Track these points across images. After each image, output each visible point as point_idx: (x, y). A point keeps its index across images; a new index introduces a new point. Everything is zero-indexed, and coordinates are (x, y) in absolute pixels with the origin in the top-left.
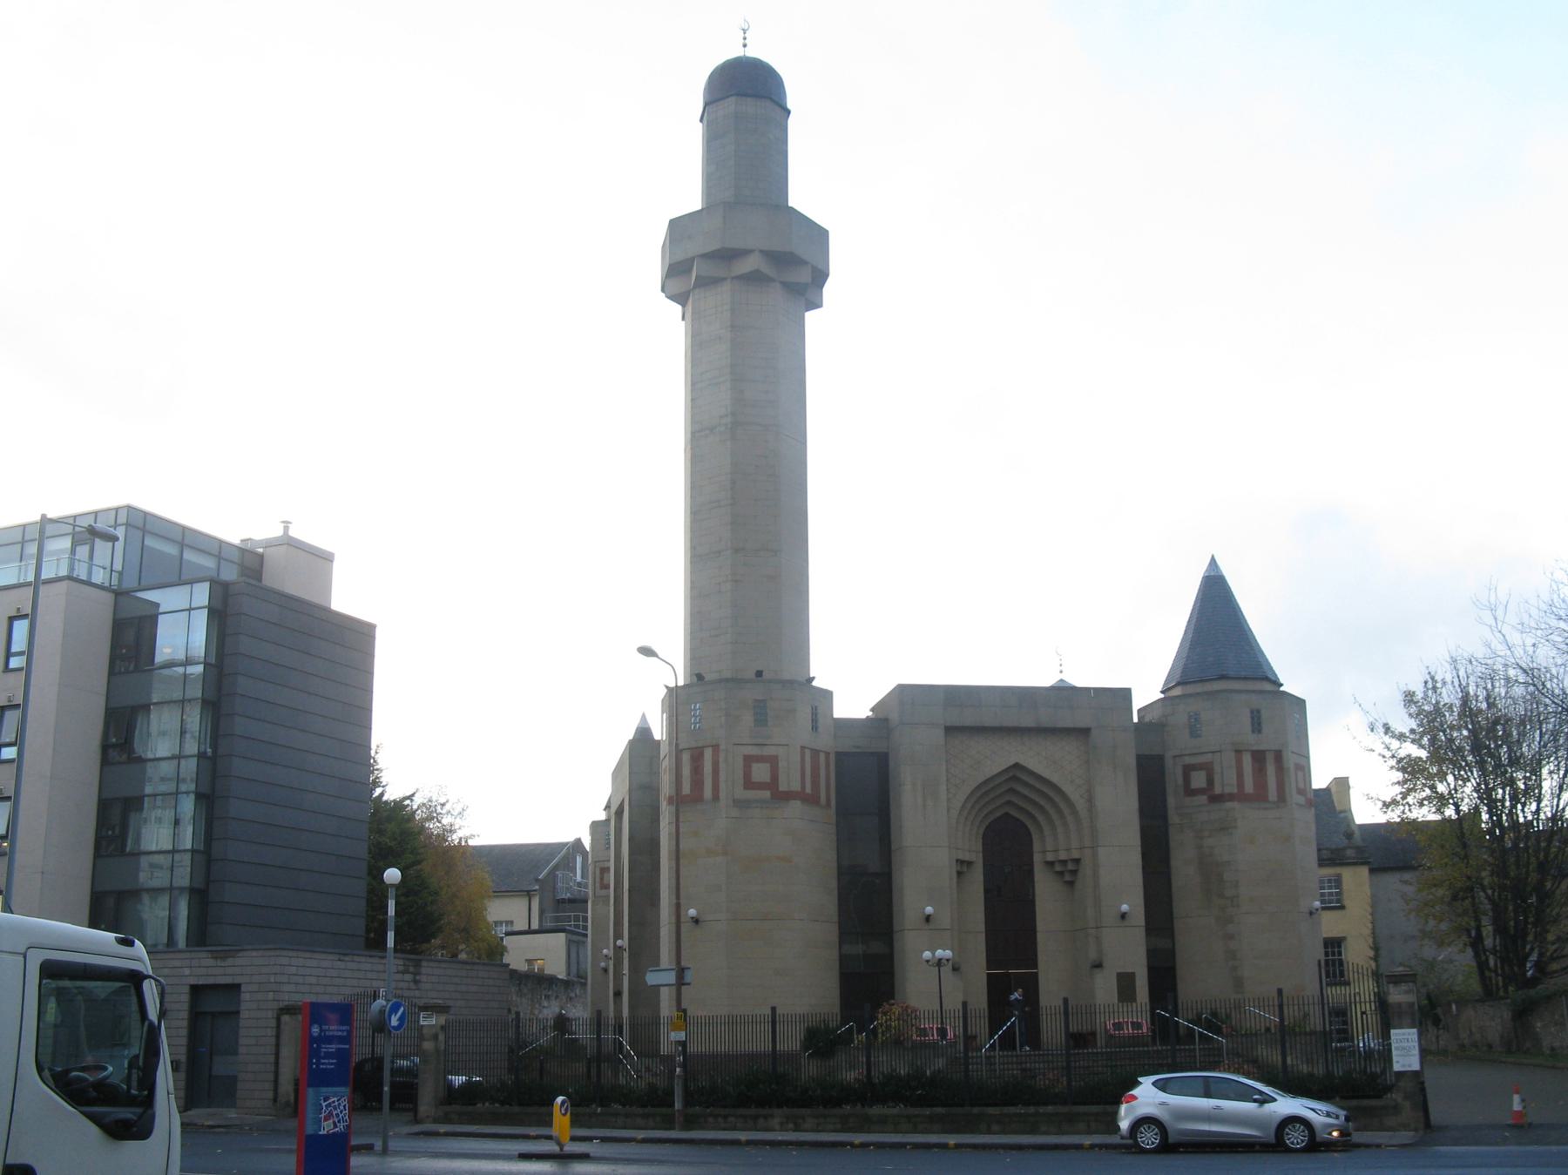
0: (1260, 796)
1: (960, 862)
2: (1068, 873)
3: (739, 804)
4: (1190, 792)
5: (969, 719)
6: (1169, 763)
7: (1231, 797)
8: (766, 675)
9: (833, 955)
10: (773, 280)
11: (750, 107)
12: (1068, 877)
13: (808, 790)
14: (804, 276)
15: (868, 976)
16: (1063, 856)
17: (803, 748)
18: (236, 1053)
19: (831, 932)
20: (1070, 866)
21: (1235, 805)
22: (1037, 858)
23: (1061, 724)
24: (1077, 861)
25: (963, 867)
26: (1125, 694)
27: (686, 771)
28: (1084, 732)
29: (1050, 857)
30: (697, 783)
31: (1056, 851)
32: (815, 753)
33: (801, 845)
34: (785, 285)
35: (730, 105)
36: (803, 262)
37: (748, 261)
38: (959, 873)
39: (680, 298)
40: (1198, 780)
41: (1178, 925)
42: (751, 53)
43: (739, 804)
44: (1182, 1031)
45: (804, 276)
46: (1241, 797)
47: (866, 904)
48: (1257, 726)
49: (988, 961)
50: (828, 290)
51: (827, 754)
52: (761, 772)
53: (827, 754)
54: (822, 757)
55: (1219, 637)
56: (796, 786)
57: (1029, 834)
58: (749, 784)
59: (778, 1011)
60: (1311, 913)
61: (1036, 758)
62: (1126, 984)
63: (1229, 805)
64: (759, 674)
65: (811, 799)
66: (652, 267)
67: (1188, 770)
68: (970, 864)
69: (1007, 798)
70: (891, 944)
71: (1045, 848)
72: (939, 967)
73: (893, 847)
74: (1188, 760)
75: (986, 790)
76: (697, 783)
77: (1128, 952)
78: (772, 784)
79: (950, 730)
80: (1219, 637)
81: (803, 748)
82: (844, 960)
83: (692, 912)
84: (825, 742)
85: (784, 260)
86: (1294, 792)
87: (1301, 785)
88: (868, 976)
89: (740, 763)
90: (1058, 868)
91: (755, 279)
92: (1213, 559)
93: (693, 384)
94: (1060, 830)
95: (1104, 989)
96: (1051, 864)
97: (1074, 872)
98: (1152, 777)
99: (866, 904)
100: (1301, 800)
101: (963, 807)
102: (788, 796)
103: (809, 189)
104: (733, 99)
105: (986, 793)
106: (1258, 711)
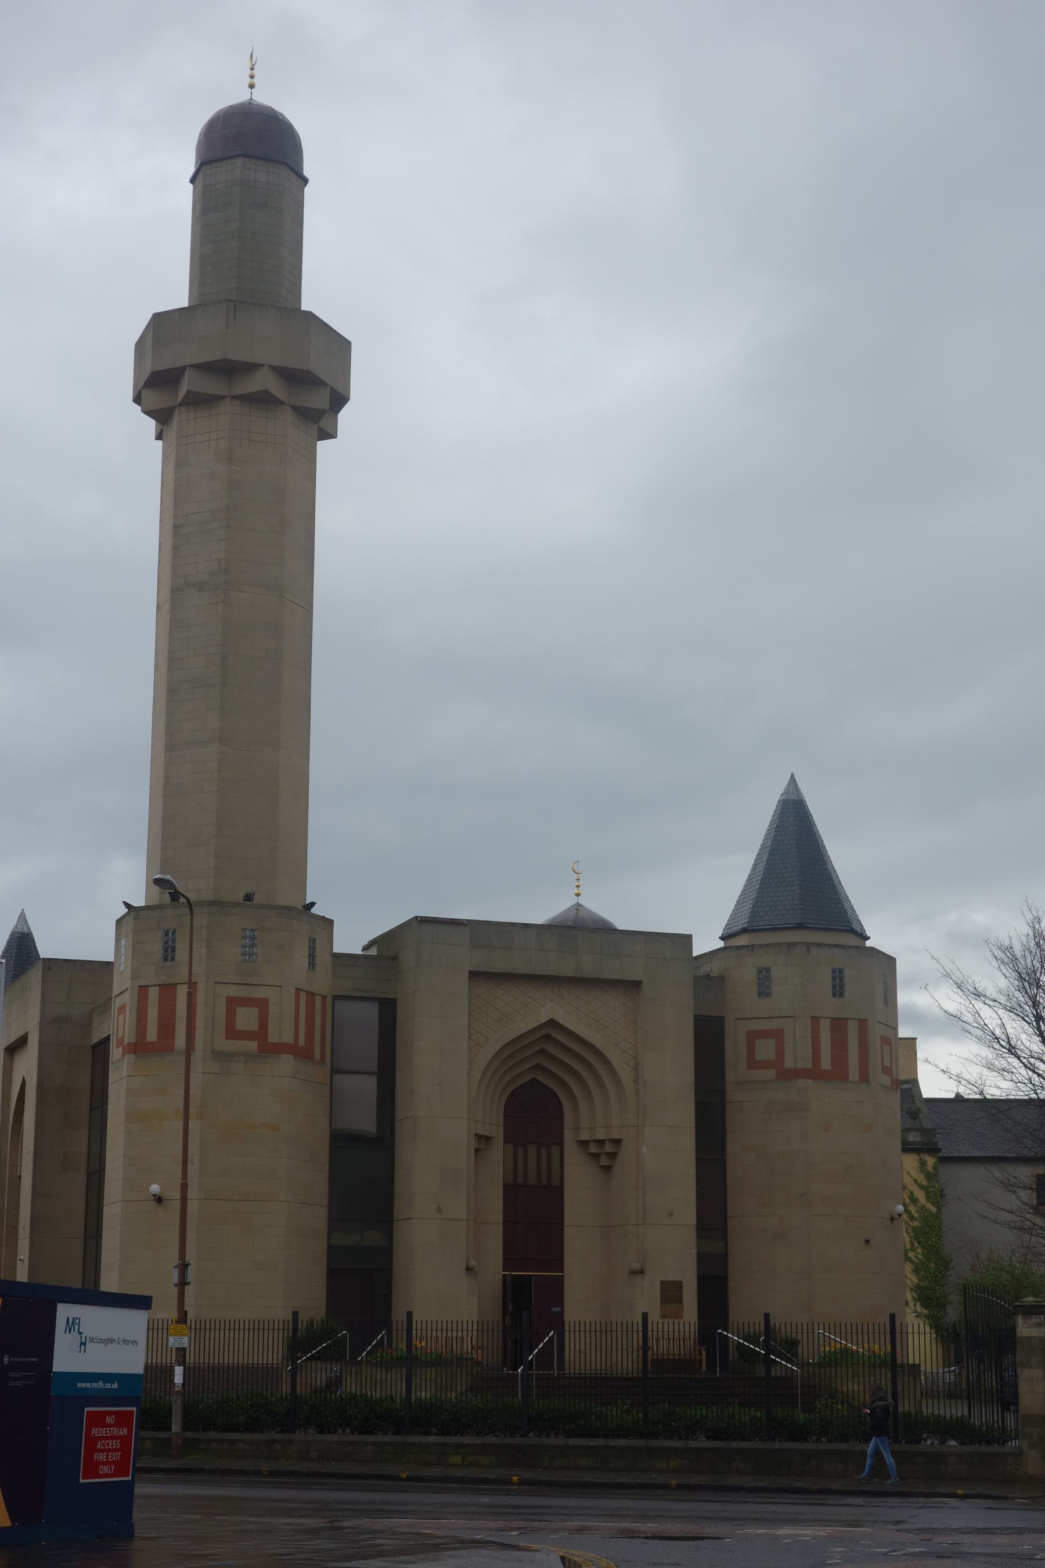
0: (838, 1074)
1: (479, 1137)
2: (605, 1155)
3: (219, 1056)
4: (753, 1063)
5: (499, 964)
6: (729, 1027)
7: (804, 1074)
8: (258, 899)
9: (321, 1246)
10: (282, 403)
11: (262, 174)
12: (604, 1161)
13: (302, 1042)
14: (320, 400)
15: (360, 1280)
16: (600, 1136)
17: (298, 990)
19: (320, 1217)
20: (609, 1148)
22: (568, 1135)
23: (607, 975)
24: (617, 1142)
25: (483, 1141)
26: (687, 940)
27: (153, 1014)
29: (584, 1136)
30: (167, 1028)
32: (311, 996)
33: (279, 1114)
34: (295, 408)
35: (236, 170)
36: (321, 383)
37: (242, 371)
38: (477, 1150)
39: (162, 417)
40: (765, 1050)
41: (731, 1223)
42: (263, 97)
43: (219, 1056)
44: (733, 1354)
45: (320, 400)
46: (814, 1073)
47: (362, 1174)
48: (838, 988)
49: (506, 1260)
50: (344, 416)
51: (324, 998)
52: (247, 1019)
53: (324, 998)
55: (797, 884)
56: (288, 1038)
57: (561, 1118)
58: (232, 1033)
60: (892, 1219)
61: (569, 1012)
62: (671, 1293)
63: (801, 1082)
65: (303, 1054)
66: (123, 375)
67: (752, 1037)
69: (534, 1062)
70: (389, 1234)
71: (584, 1120)
72: (445, 1281)
73: (399, 1115)
74: (754, 1025)
76: (167, 1028)
77: (677, 1258)
78: (261, 1034)
80: (797, 884)
81: (298, 990)
82: (333, 1251)
84: (323, 983)
85: (297, 378)
86: (879, 1069)
87: (887, 1063)
88: (360, 1280)
89: (222, 1007)
90: (593, 1149)
91: (262, 400)
92: (792, 775)
93: (176, 527)
94: (595, 1091)
95: (646, 1299)
96: (584, 1144)
97: (613, 1156)
98: (709, 1037)
99: (362, 1174)
100: (886, 1080)
101: (484, 1073)
102: (279, 1049)
103: (327, 285)
104: (239, 161)
105: (511, 1056)
106: (841, 971)
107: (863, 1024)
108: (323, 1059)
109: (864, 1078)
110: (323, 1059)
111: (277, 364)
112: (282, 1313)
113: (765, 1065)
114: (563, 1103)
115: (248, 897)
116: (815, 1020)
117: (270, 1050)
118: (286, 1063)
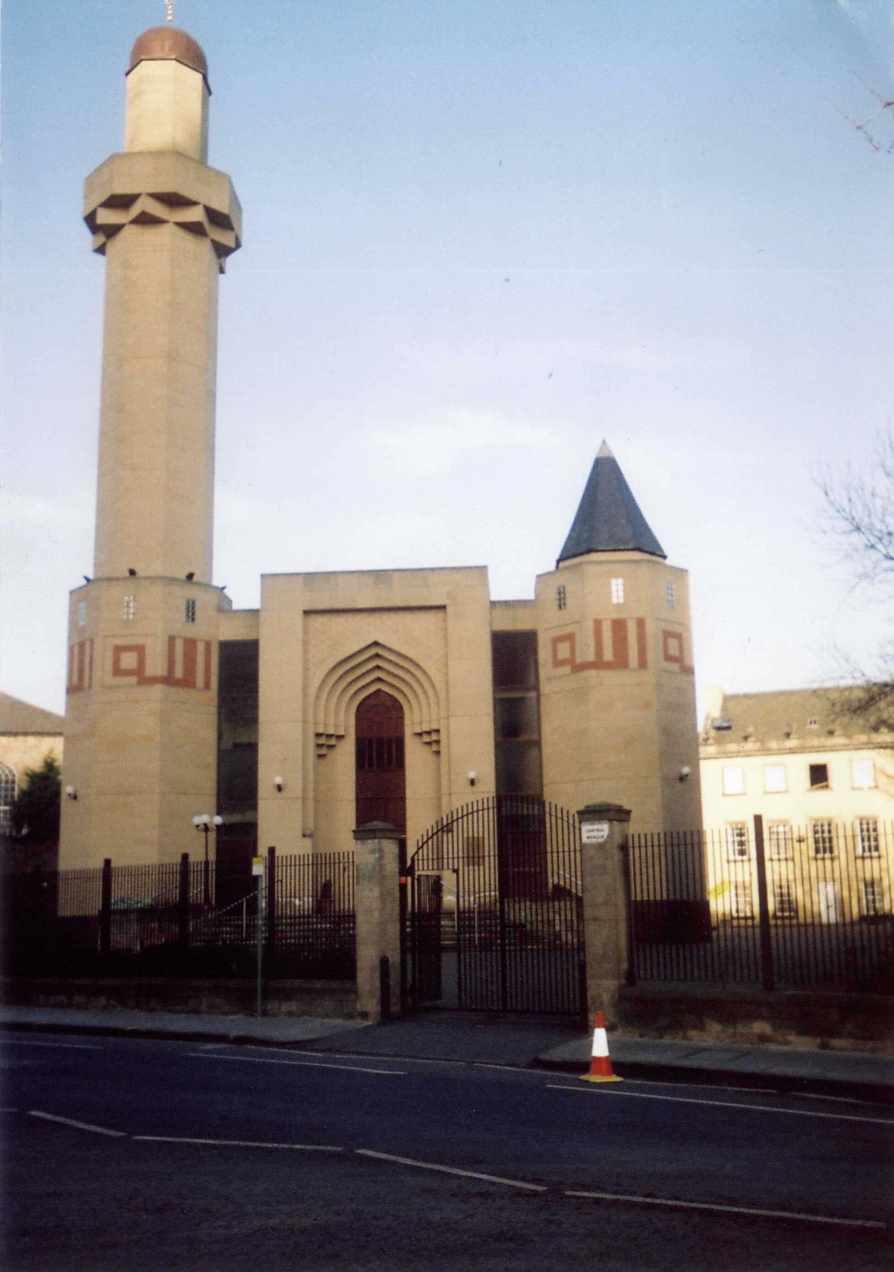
0: (621, 662)
8: (140, 573)
16: (331, 732)
18: (709, 939)
20: (333, 742)
21: (592, 673)
24: (321, 756)
25: (325, 744)
28: (443, 608)
31: (430, 722)
32: (190, 644)
46: (599, 664)
54: (201, 647)
57: (401, 708)
58: (118, 671)
59: (278, 853)
61: (387, 631)
64: (190, 576)
68: (340, 737)
75: (347, 666)
78: (139, 672)
79: (307, 613)
83: (278, 780)
89: (110, 654)
90: (322, 741)
106: (193, 602)
107: (641, 623)
108: (207, 686)
109: (643, 664)
110: (207, 686)
111: (152, 191)
112: (660, 829)
113: (128, 673)
114: (404, 707)
115: (190, 576)
116: (172, 640)
117: (145, 681)
118: (157, 691)
